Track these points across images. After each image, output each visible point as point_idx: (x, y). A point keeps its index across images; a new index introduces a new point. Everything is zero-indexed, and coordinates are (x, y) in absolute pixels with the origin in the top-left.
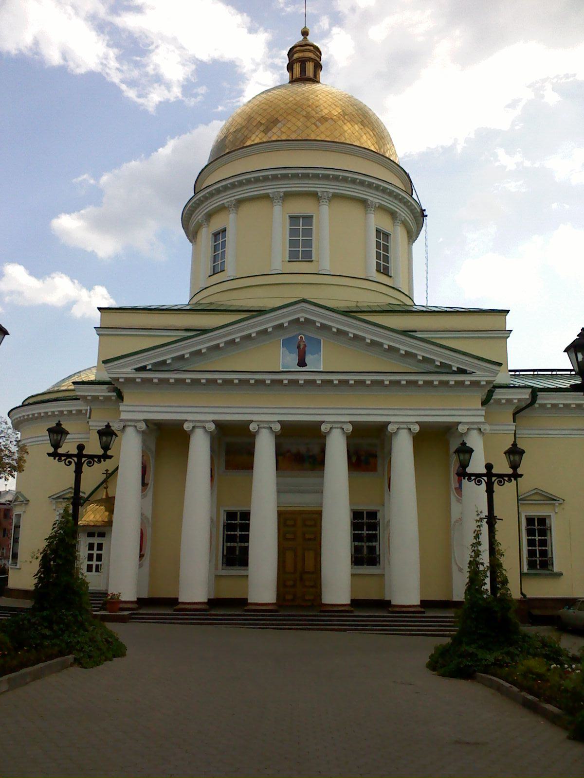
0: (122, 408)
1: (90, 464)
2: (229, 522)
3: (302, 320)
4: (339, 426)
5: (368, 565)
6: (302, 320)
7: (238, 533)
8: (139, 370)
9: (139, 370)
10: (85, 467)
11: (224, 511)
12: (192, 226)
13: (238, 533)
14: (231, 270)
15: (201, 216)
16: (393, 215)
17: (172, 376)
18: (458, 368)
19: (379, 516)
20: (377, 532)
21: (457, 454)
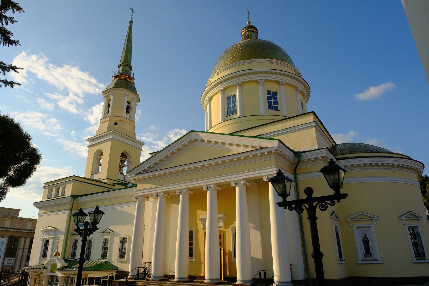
10: (319, 212)
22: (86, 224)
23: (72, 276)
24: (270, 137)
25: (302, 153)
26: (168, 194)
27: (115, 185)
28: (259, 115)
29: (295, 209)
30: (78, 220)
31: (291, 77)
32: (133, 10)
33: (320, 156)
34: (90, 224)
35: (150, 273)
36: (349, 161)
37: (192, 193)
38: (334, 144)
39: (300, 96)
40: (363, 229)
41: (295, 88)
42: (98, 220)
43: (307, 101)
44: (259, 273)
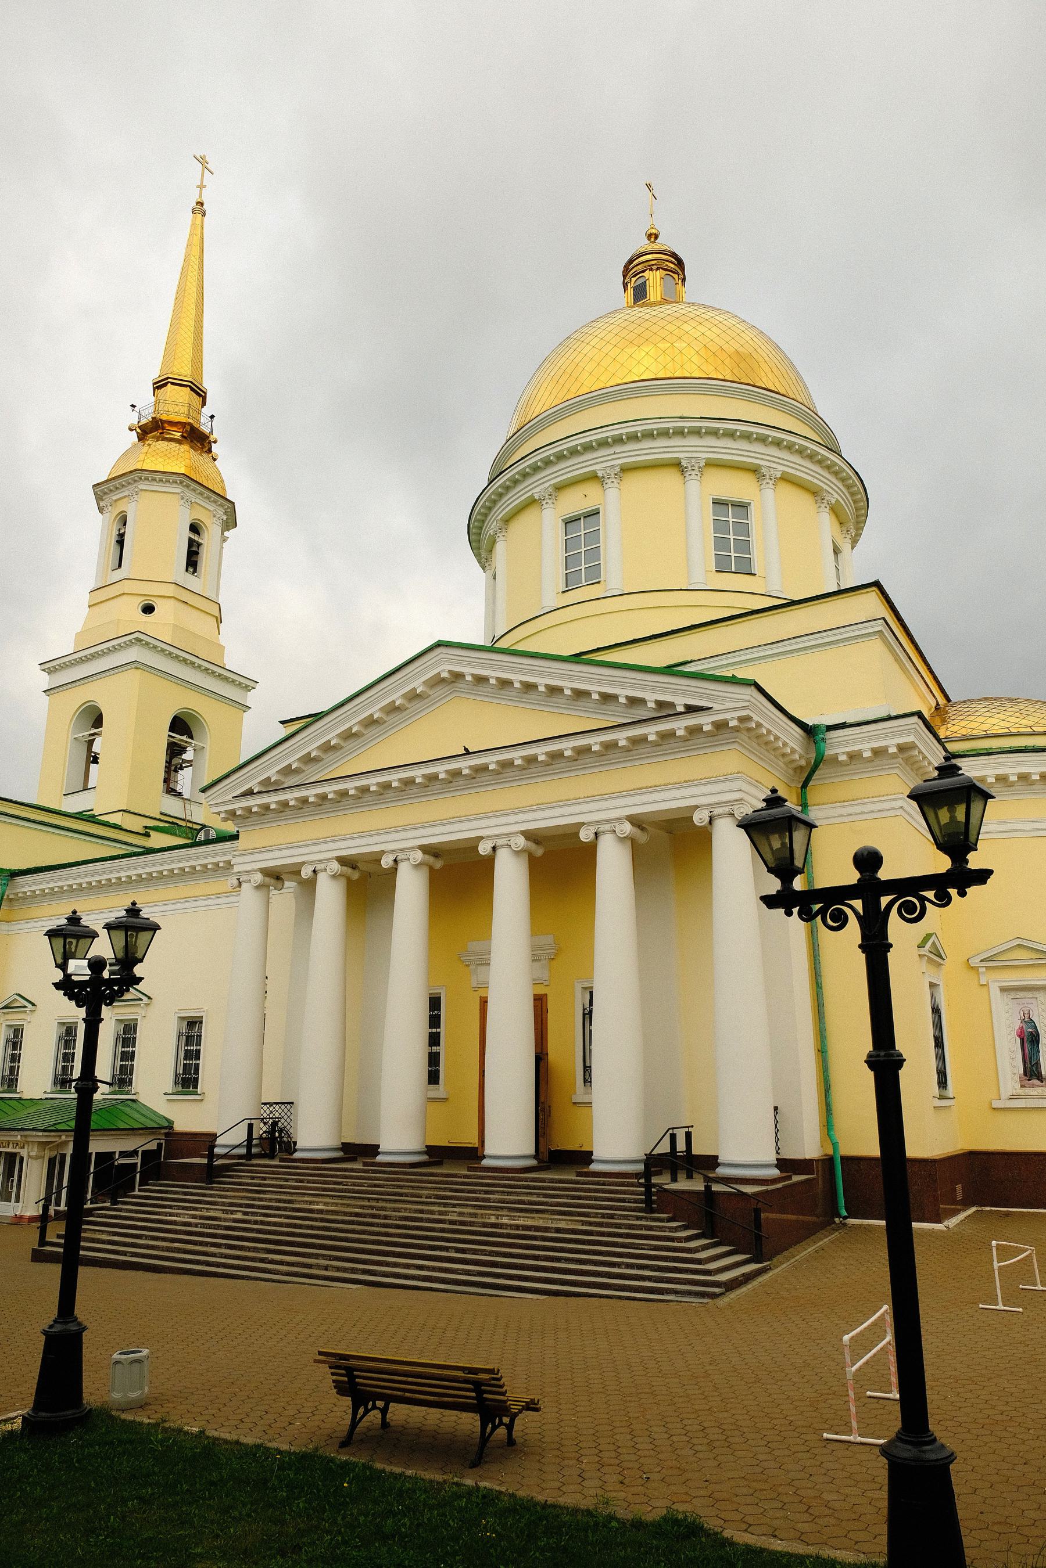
1: (913, 914)
10: (896, 927)
17: (291, 797)
22: (96, 965)
23: (10, 1150)
24: (720, 670)
25: (831, 732)
26: (354, 867)
27: (152, 833)
28: (681, 590)
29: (819, 917)
30: (787, 834)
31: (801, 452)
32: (202, 161)
33: (891, 744)
34: (111, 965)
35: (289, 1136)
36: (992, 761)
37: (438, 864)
38: (942, 701)
39: (826, 522)
40: (1022, 994)
41: (814, 493)
42: (139, 950)
43: (854, 542)
44: (668, 1135)
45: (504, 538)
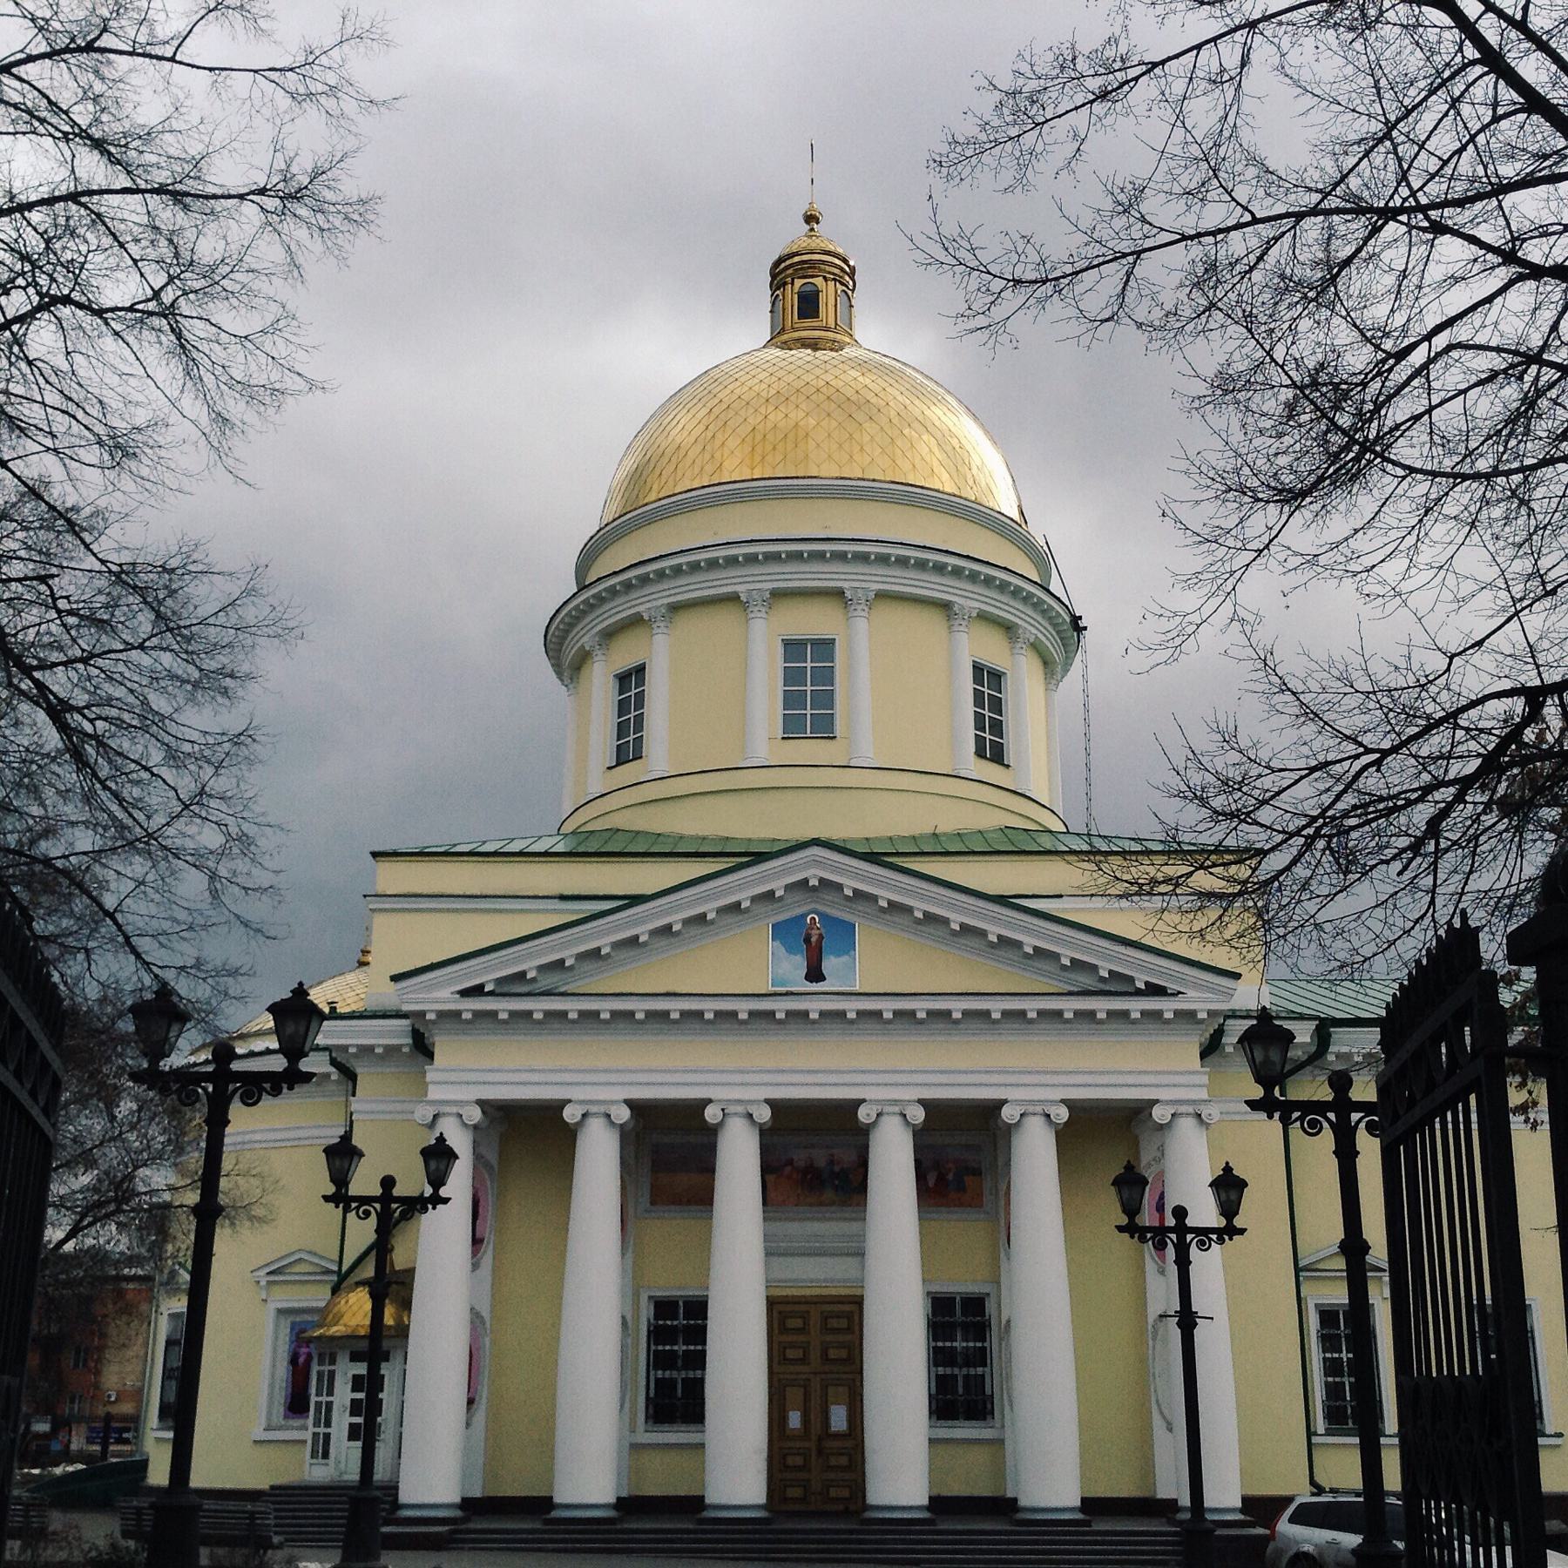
0: (430, 1077)
2: (661, 1322)
3: (813, 882)
4: (897, 1109)
5: (967, 1418)
6: (813, 882)
7: (680, 1348)
8: (465, 993)
9: (465, 993)
10: (1194, 1252)
11: (650, 1298)
12: (570, 653)
13: (680, 1348)
14: (659, 753)
15: (588, 636)
16: (1009, 629)
17: (539, 1006)
18: (1147, 983)
19: (990, 1307)
20: (933, 1344)
21: (1246, 1044)
45: (603, 658)
